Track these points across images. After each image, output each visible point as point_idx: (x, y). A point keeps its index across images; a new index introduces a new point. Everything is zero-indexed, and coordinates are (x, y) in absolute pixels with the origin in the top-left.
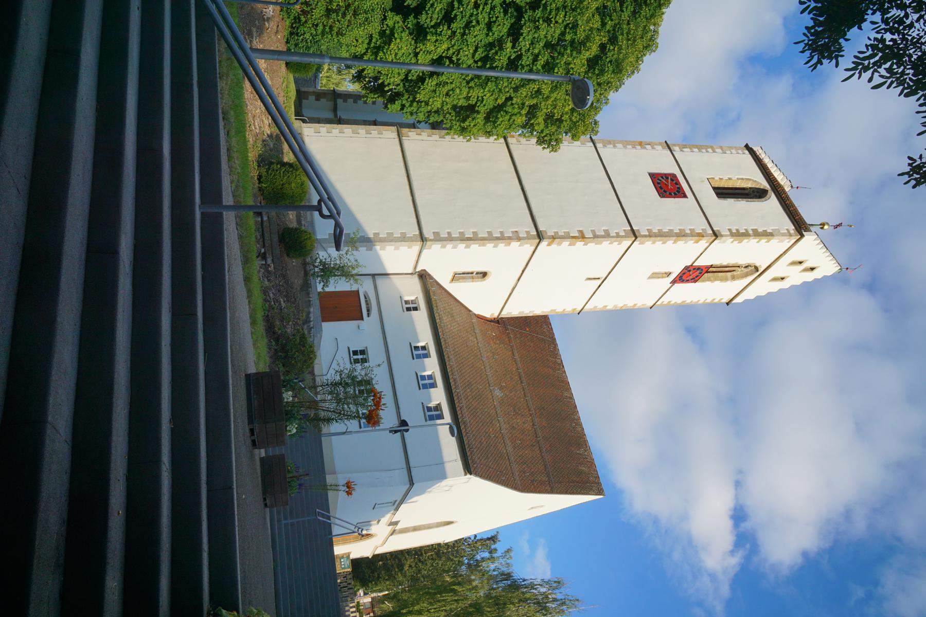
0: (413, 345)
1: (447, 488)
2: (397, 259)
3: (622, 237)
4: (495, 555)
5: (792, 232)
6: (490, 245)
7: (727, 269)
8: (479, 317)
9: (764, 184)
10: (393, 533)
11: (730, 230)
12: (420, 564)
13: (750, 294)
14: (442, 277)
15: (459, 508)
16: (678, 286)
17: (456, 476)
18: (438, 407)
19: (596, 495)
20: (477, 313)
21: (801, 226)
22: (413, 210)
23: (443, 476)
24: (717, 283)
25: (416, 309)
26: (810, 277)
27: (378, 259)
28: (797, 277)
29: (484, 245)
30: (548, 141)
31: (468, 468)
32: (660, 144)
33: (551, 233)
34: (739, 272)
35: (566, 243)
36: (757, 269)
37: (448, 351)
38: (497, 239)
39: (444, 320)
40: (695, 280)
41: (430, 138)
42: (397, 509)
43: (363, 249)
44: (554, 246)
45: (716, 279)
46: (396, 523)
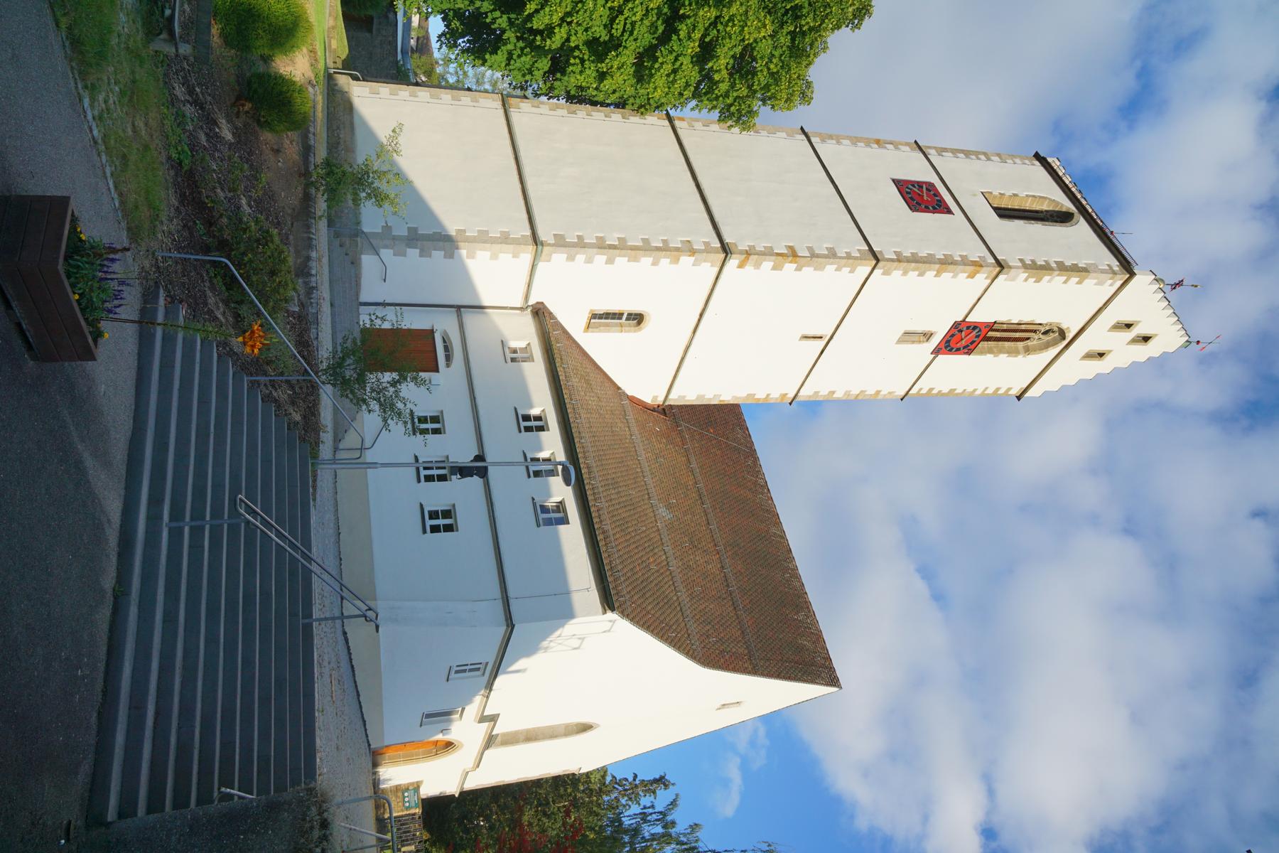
0: (521, 412)
1: (576, 643)
2: (496, 277)
3: (856, 258)
4: (673, 831)
5: (1116, 269)
6: (647, 261)
7: (1017, 335)
8: (633, 400)
9: (1068, 205)
10: (490, 741)
11: (1021, 260)
12: (544, 819)
13: (1049, 383)
14: (572, 320)
15: (597, 694)
16: (943, 359)
17: (588, 614)
18: (560, 507)
19: (827, 685)
20: (629, 393)
21: (1127, 266)
22: (522, 202)
23: (566, 613)
24: (1003, 356)
25: (541, 429)
26: (1142, 353)
27: (464, 277)
28: (1124, 354)
29: (636, 259)
30: (736, 114)
31: (608, 601)
32: (907, 144)
33: (743, 246)
34: (1035, 340)
35: (768, 264)
36: (1062, 334)
37: (581, 423)
38: (658, 249)
39: (573, 383)
40: (968, 350)
41: (552, 113)
42: (489, 686)
43: (438, 255)
44: (749, 268)
45: (1001, 351)
46: (493, 719)
